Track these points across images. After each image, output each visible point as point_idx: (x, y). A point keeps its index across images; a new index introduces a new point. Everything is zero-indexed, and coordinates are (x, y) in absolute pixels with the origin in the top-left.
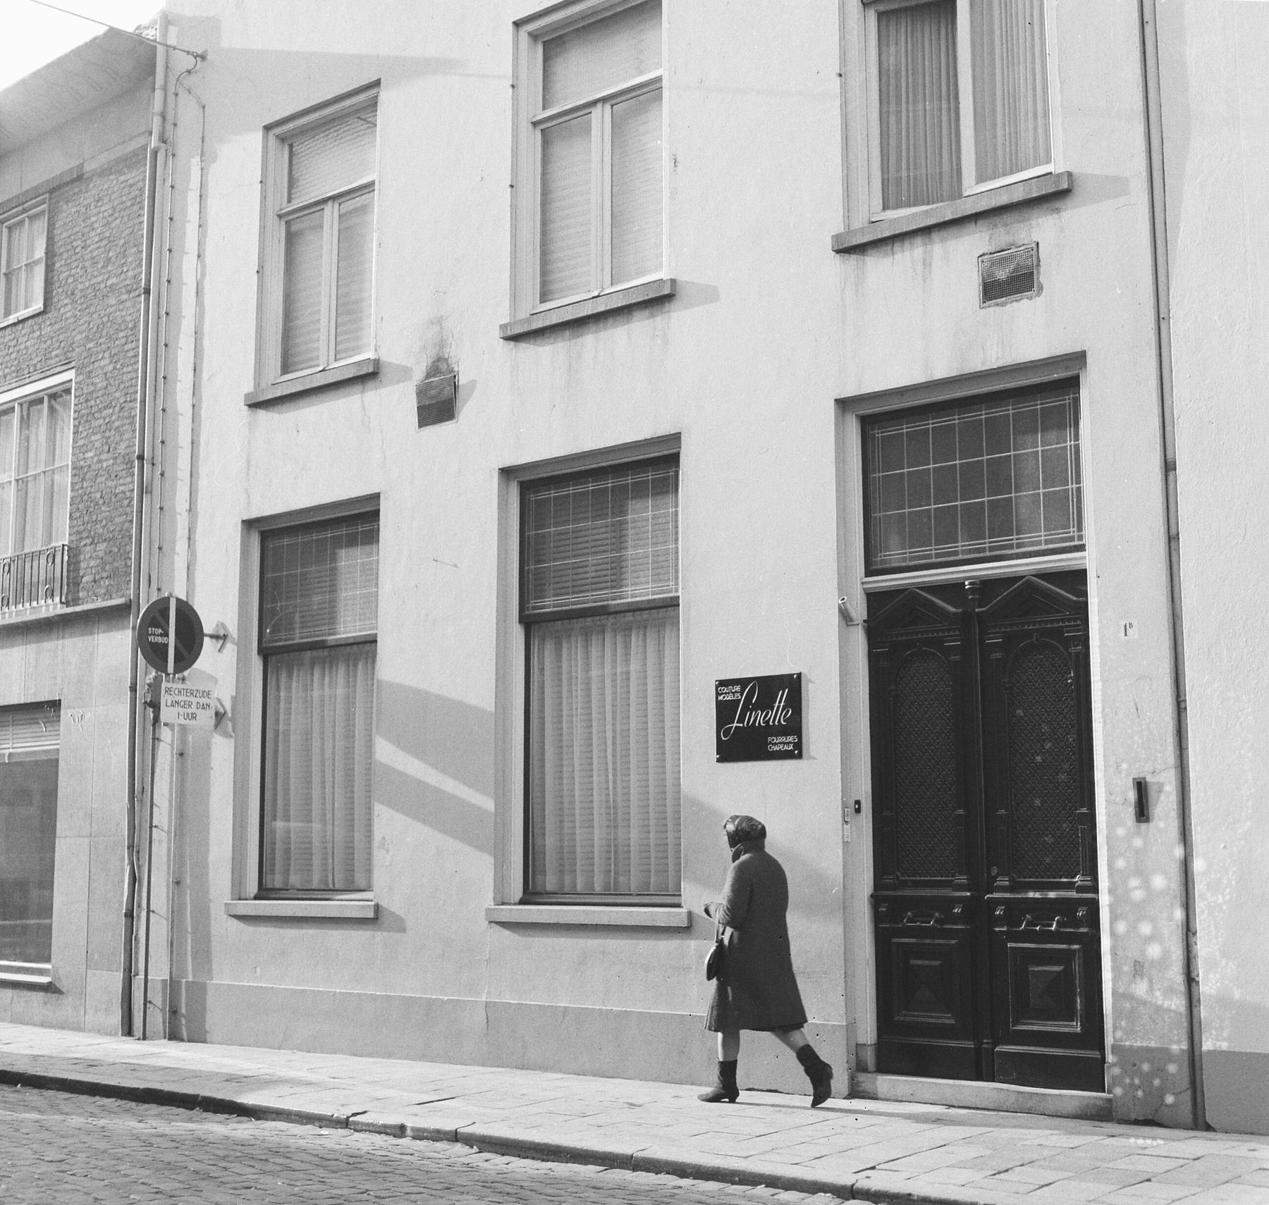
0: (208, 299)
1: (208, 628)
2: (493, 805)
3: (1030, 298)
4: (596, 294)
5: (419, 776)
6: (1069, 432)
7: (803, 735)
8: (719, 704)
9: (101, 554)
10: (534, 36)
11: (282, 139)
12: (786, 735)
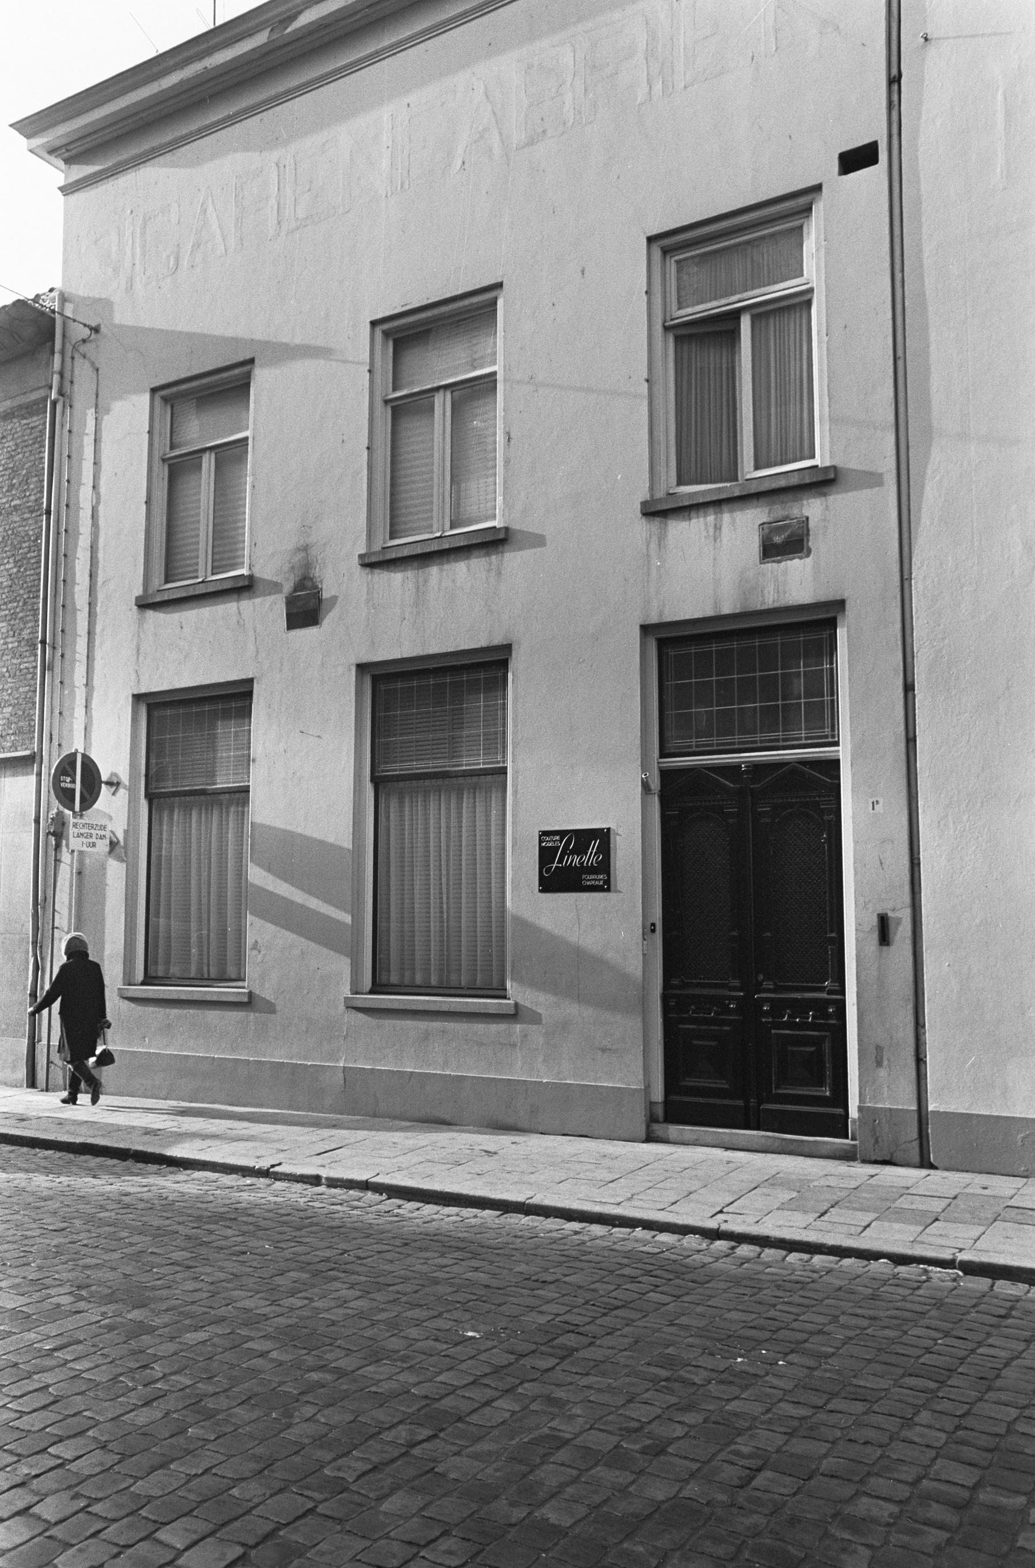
0: (102, 522)
1: (104, 778)
2: (350, 918)
3: (801, 558)
4: (438, 534)
5: (286, 895)
6: (826, 660)
7: (612, 872)
8: (541, 848)
9: (7, 715)
10: (386, 334)
11: (165, 400)
12: (597, 873)
